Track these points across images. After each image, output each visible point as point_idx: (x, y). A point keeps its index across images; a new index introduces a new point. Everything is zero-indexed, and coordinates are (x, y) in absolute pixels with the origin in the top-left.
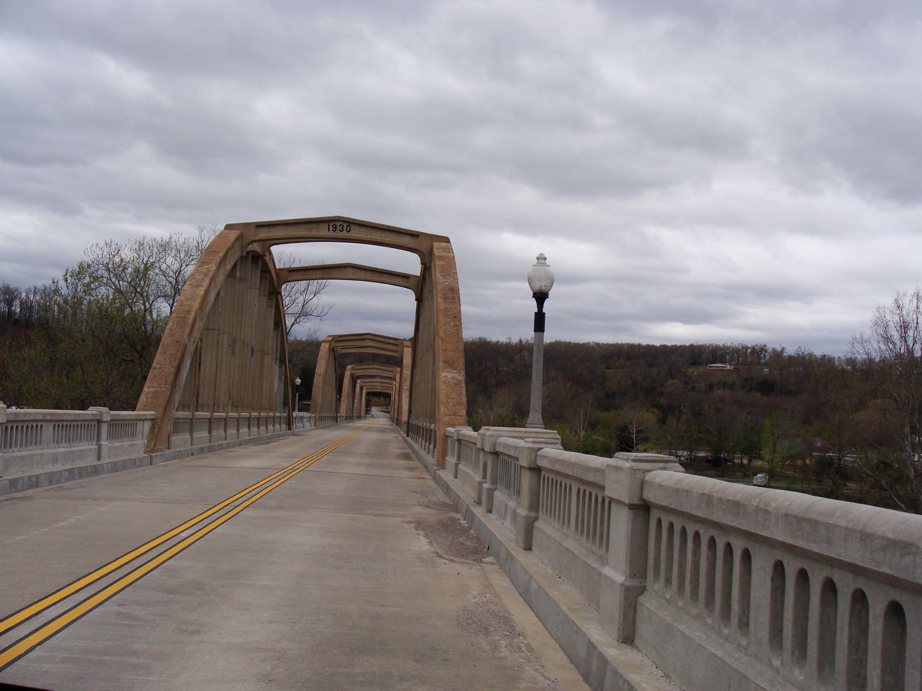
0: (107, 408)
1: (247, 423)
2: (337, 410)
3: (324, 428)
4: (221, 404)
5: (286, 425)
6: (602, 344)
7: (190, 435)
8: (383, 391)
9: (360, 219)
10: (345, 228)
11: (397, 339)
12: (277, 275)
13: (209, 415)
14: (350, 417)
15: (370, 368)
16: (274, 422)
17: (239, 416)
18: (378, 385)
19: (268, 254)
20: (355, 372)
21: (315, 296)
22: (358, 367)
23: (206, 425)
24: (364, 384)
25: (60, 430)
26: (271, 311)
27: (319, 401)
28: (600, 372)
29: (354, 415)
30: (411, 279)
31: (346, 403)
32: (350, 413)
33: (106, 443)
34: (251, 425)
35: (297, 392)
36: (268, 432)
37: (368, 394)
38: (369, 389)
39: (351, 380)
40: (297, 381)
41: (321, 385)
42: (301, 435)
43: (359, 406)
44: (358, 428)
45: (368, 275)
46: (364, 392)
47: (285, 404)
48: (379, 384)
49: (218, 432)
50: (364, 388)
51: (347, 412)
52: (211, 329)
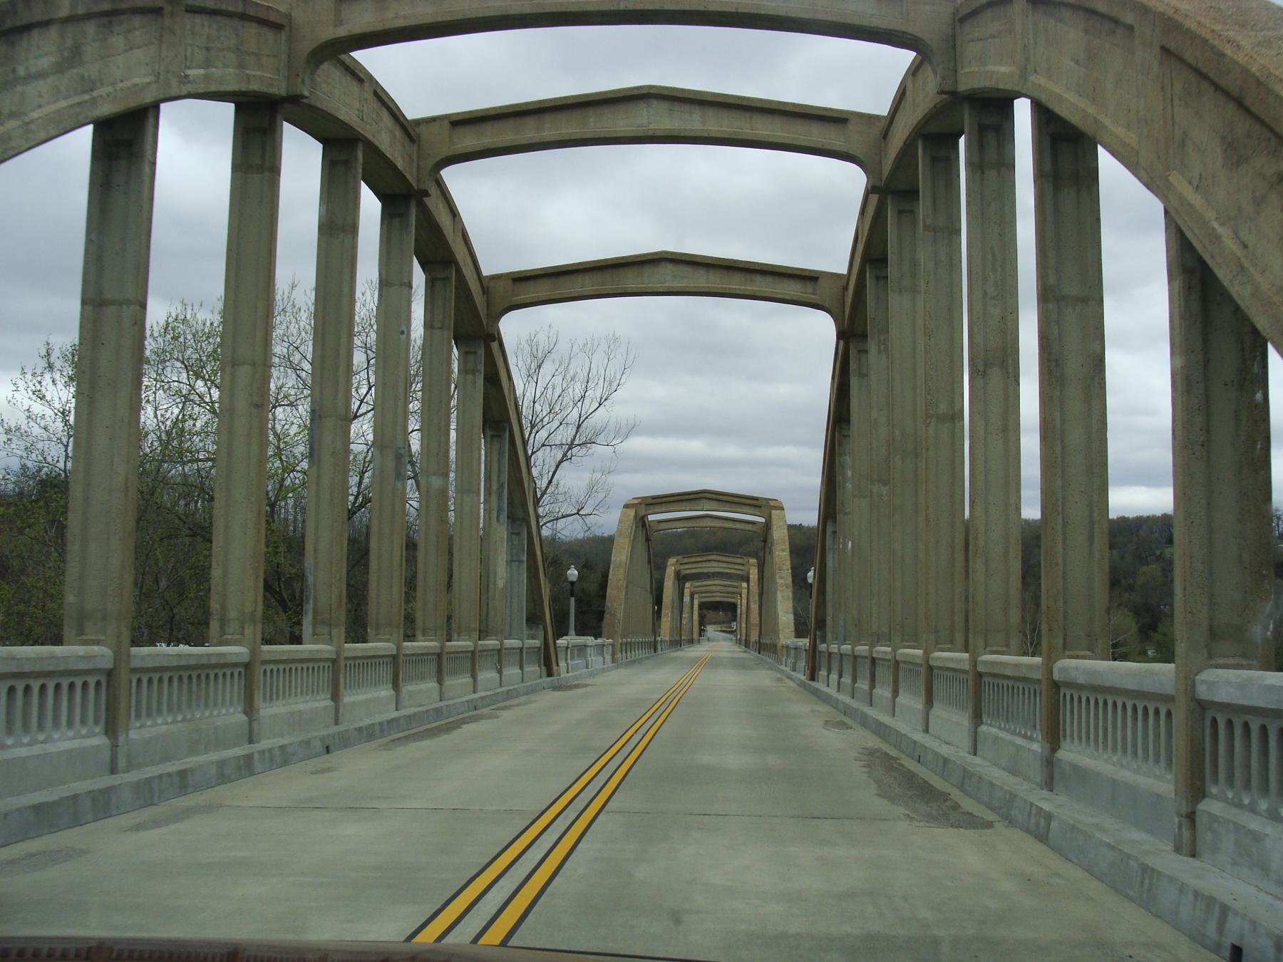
1: (434, 667)
2: (655, 630)
3: (633, 663)
4: (232, 614)
5: (540, 666)
6: (1033, 520)
7: (245, 713)
8: (726, 600)
11: (756, 499)
12: (485, 291)
13: (436, 647)
14: (677, 641)
15: (705, 561)
16: (500, 661)
17: (338, 653)
18: (716, 590)
19: (433, 191)
20: (682, 567)
21: (600, 405)
22: (686, 560)
23: (387, 672)
24: (695, 589)
25: (369, 667)
26: (474, 382)
27: (620, 615)
28: (1035, 561)
29: (683, 638)
30: (822, 282)
31: (669, 619)
32: (677, 635)
34: (445, 670)
35: (572, 596)
36: (479, 687)
37: (702, 606)
38: (702, 597)
39: (677, 582)
40: (572, 574)
41: (623, 583)
42: (577, 686)
43: (691, 624)
44: (695, 661)
45: (715, 279)
46: (696, 602)
47: (534, 619)
48: (718, 588)
49: (487, 675)
50: (696, 596)
51: (671, 635)
52: (113, 302)
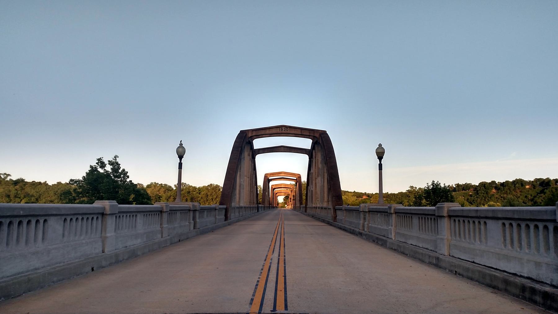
0: (115, 201)
9: (338, 168)
10: (286, 129)
33: (167, 225)
